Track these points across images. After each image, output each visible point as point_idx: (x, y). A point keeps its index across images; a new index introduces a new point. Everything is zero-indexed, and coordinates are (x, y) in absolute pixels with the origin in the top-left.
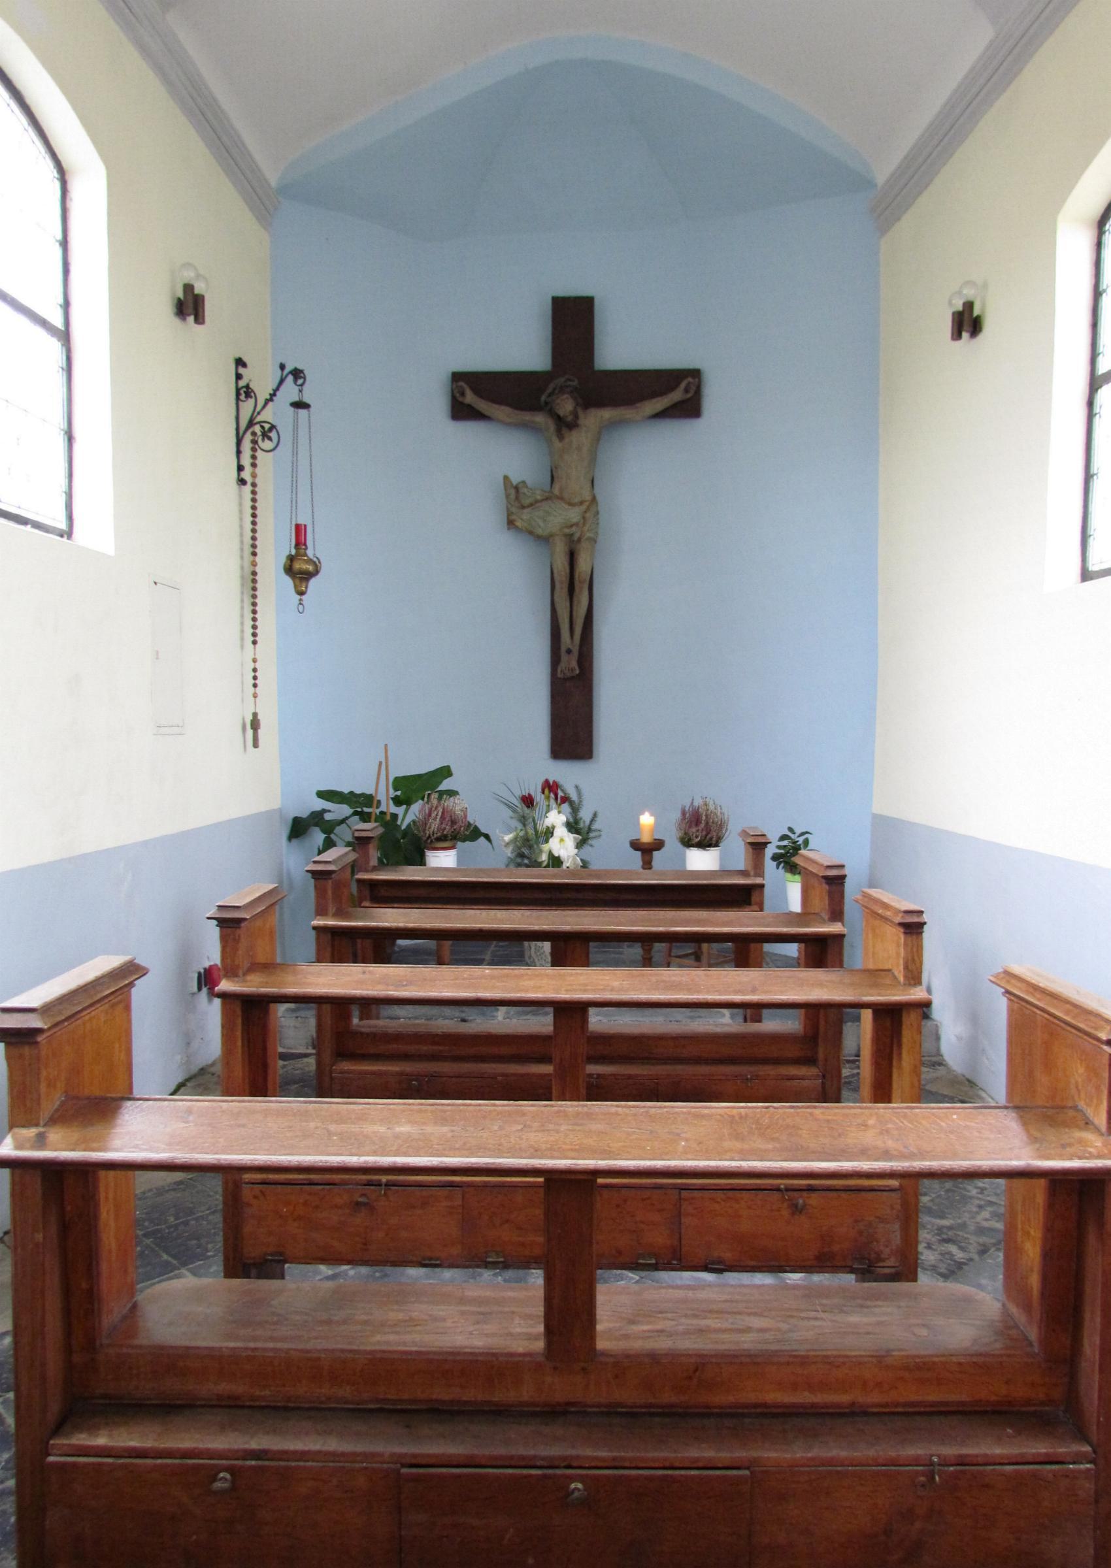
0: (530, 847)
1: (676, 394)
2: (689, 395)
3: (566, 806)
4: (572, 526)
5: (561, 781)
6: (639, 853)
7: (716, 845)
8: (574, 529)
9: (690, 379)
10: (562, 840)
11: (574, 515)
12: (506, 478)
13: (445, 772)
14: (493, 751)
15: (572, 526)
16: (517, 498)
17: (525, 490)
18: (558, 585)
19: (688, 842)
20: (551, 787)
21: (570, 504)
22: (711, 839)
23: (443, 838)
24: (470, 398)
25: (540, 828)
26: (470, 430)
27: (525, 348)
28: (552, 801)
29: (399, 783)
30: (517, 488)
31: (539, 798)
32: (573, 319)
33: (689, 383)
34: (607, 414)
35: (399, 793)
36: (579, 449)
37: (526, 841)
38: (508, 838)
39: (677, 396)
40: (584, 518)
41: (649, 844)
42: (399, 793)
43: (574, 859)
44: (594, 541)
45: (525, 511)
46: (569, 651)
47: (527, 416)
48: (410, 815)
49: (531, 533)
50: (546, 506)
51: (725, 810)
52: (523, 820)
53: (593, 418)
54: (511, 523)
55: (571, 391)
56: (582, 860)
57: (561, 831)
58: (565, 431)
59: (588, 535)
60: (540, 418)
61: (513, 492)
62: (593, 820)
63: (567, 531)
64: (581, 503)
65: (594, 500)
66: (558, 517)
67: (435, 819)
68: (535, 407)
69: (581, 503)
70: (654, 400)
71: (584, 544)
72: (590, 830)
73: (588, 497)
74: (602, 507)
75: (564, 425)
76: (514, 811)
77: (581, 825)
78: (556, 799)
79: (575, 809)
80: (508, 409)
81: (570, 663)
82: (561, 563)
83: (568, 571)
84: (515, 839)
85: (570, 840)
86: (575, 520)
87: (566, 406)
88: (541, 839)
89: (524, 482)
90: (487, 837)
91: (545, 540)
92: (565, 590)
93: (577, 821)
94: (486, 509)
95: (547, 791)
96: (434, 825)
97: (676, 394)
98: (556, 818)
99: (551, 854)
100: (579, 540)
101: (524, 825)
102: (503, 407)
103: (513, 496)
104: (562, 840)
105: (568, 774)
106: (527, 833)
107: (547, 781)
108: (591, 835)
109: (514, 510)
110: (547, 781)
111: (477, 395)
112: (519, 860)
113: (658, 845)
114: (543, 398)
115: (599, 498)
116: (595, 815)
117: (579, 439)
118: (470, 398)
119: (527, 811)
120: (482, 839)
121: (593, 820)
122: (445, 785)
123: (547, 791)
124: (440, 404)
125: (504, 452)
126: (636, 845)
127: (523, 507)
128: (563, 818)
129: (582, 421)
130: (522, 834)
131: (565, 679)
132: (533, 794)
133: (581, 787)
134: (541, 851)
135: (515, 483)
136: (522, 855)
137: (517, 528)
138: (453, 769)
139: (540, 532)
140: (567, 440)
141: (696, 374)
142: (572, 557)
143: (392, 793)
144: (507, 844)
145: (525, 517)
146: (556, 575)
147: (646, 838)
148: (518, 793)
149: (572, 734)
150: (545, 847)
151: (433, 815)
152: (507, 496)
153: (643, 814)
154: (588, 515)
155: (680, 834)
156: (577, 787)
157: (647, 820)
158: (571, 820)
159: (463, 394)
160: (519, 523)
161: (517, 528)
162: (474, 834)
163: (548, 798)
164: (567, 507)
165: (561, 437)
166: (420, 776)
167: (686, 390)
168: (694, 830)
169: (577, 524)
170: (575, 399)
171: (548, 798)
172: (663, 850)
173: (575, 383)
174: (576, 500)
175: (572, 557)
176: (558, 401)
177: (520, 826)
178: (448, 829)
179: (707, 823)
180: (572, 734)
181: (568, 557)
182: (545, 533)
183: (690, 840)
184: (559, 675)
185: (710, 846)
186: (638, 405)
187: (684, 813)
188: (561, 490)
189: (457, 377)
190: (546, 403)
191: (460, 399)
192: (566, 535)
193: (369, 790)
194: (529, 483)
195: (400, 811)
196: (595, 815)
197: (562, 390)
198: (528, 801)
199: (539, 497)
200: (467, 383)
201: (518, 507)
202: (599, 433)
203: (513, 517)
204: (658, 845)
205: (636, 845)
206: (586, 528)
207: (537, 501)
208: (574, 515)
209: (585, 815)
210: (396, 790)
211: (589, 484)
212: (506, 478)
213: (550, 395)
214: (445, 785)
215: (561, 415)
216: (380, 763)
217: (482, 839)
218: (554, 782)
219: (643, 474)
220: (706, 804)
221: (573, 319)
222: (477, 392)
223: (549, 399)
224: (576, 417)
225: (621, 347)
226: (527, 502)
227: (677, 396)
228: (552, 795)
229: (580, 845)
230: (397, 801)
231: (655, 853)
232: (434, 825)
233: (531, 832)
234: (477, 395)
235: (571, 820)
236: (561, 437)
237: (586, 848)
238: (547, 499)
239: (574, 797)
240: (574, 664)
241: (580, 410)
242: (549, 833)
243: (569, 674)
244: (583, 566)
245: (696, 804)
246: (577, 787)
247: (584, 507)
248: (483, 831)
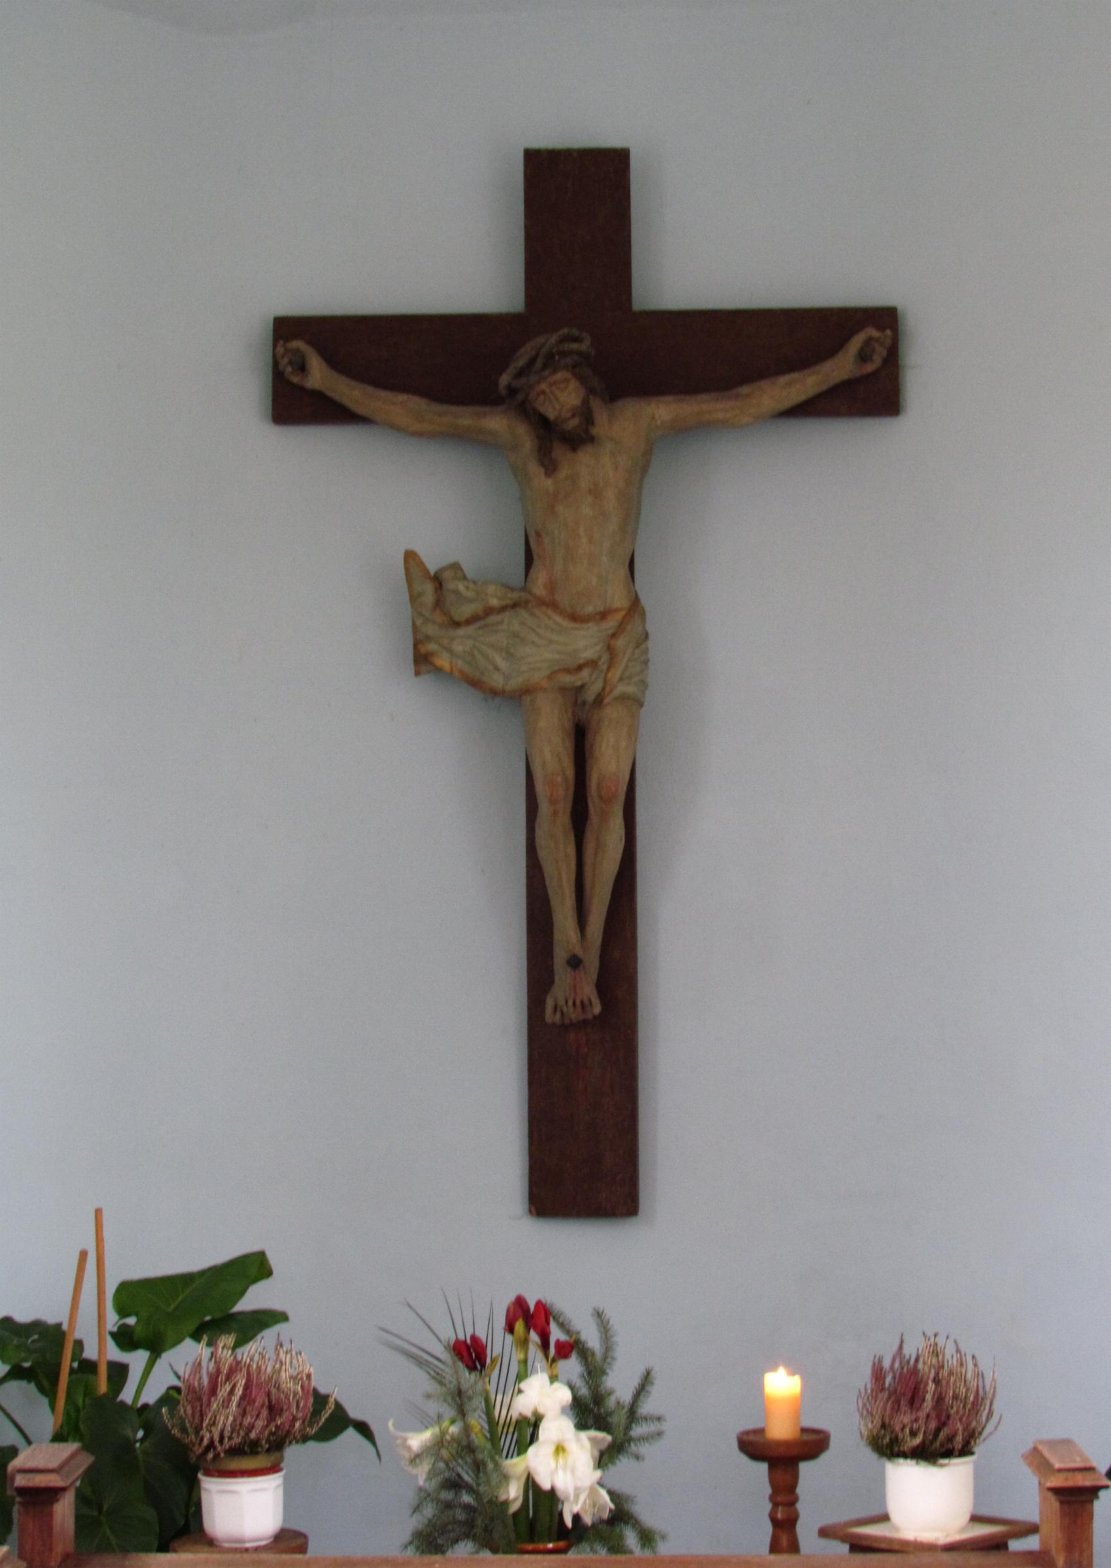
0: (478, 1467)
1: (837, 363)
2: (870, 368)
3: (572, 1366)
4: (580, 668)
5: (558, 1301)
6: (763, 1467)
7: (966, 1451)
8: (585, 673)
9: (875, 333)
10: (560, 1449)
11: (585, 642)
12: (410, 557)
13: (255, 1267)
14: (383, 1210)
15: (580, 668)
16: (439, 603)
17: (461, 586)
18: (544, 808)
19: (889, 1447)
20: (530, 1318)
21: (575, 618)
22: (950, 1439)
23: (248, 1448)
24: (319, 375)
25: (500, 1413)
26: (318, 448)
27: (455, 256)
28: (534, 1351)
29: (132, 1295)
30: (438, 580)
31: (499, 1344)
32: (577, 201)
33: (869, 342)
34: (663, 410)
35: (131, 1321)
36: (596, 492)
37: (465, 1448)
38: (417, 1440)
39: (841, 367)
40: (610, 649)
41: (787, 1444)
42: (131, 1321)
43: (592, 1491)
44: (635, 703)
45: (461, 632)
46: (575, 962)
47: (465, 417)
48: (151, 1379)
49: (475, 683)
50: (512, 622)
51: (985, 1365)
52: (459, 1399)
53: (629, 423)
54: (422, 661)
55: (571, 357)
56: (611, 1493)
57: (557, 1427)
58: (559, 451)
59: (621, 688)
60: (497, 422)
61: (429, 588)
62: (642, 1390)
63: (568, 679)
64: (603, 615)
65: (635, 607)
66: (544, 649)
67: (227, 1402)
68: (484, 396)
69: (603, 615)
70: (783, 380)
71: (612, 712)
72: (632, 1414)
73: (619, 601)
74: (654, 622)
75: (557, 440)
76: (438, 1379)
77: (611, 1403)
78: (545, 1345)
79: (594, 1371)
80: (417, 403)
81: (576, 991)
82: (553, 755)
83: (570, 773)
84: (439, 1443)
85: (581, 1448)
86: (589, 654)
87: (563, 396)
88: (506, 1442)
89: (456, 567)
90: (364, 1429)
91: (516, 698)
92: (565, 819)
93: (598, 1398)
94: (361, 630)
95: (519, 1326)
96: (224, 1417)
97: (837, 363)
98: (544, 1394)
99: (530, 1483)
100: (599, 701)
101: (462, 1412)
102: (402, 397)
103: (429, 598)
104: (560, 1449)
105: (574, 1265)
106: (467, 1429)
107: (520, 1302)
108: (637, 1431)
109: (430, 630)
110: (520, 1302)
111: (334, 368)
112: (447, 1495)
113: (813, 1444)
114: (504, 380)
115: (645, 601)
116: (646, 1380)
117: (595, 467)
118: (319, 375)
119: (468, 1378)
120: (351, 1433)
121: (642, 1390)
122: (254, 1299)
123: (519, 1326)
124: (249, 389)
125: (414, 496)
126: (753, 1446)
127: (457, 624)
128: (564, 1395)
129: (602, 425)
130: (454, 1429)
131: (566, 1027)
132: (482, 1335)
133: (608, 1313)
134: (506, 1478)
135: (432, 569)
136: (454, 1484)
137: (438, 670)
138: (273, 1260)
139: (497, 681)
140: (563, 473)
141: (885, 319)
142: (581, 740)
143: (112, 1320)
144: (416, 1459)
145: (458, 648)
146: (539, 787)
147: (780, 1430)
148: (449, 1335)
149: (584, 1146)
150: (516, 1465)
151: (223, 1392)
152: (414, 598)
153: (774, 1368)
154: (620, 643)
155: (873, 1425)
156: (599, 1314)
157: (782, 1385)
158: (584, 1391)
159: (302, 368)
160: (443, 661)
161: (438, 670)
162: (331, 1420)
163: (524, 1343)
164: (566, 623)
165: (550, 467)
166: (186, 1279)
167: (863, 356)
168: (906, 1419)
169: (592, 664)
170: (582, 379)
171: (524, 1343)
172: (824, 1457)
173: (585, 346)
174: (590, 609)
175: (581, 740)
176: (543, 386)
177: (449, 1412)
178: (259, 1427)
179: (939, 1399)
180: (584, 1146)
181: (569, 744)
182: (515, 683)
183: (895, 1441)
184: (549, 1016)
185: (949, 1454)
186: (745, 390)
187: (878, 1374)
188: (552, 586)
189: (287, 329)
190: (512, 391)
191: (295, 379)
192: (563, 690)
193: (53, 1311)
194: (468, 569)
195: (137, 1360)
196: (646, 1380)
197: (550, 361)
198: (471, 1354)
199: (494, 602)
200: (310, 343)
201: (440, 622)
202: (648, 453)
203: (432, 647)
204: (813, 1444)
205: (753, 1446)
206: (615, 674)
207: (489, 611)
208: (585, 642)
209: (620, 1384)
210: (122, 1312)
211: (623, 571)
212: (410, 557)
213: (520, 374)
214: (254, 1299)
215: (551, 415)
216: (83, 1255)
217: (351, 1433)
218: (539, 1304)
219: (752, 538)
220: (935, 1352)
221: (577, 201)
222: (333, 362)
223: (516, 384)
224: (588, 419)
225: (698, 252)
226: (467, 610)
227: (841, 367)
228: (534, 1336)
229: (605, 1458)
230: (125, 1339)
231: (805, 1468)
232: (224, 1417)
233: (477, 1421)
234: (334, 368)
235: (584, 1391)
236: (550, 467)
237: (624, 1464)
238: (515, 606)
239: (592, 1338)
240: (588, 991)
241: (596, 404)
242: (528, 1430)
243: (574, 1015)
244: (608, 761)
245: (910, 1351)
246: (599, 1314)
247: (611, 624)
248: (354, 1413)
